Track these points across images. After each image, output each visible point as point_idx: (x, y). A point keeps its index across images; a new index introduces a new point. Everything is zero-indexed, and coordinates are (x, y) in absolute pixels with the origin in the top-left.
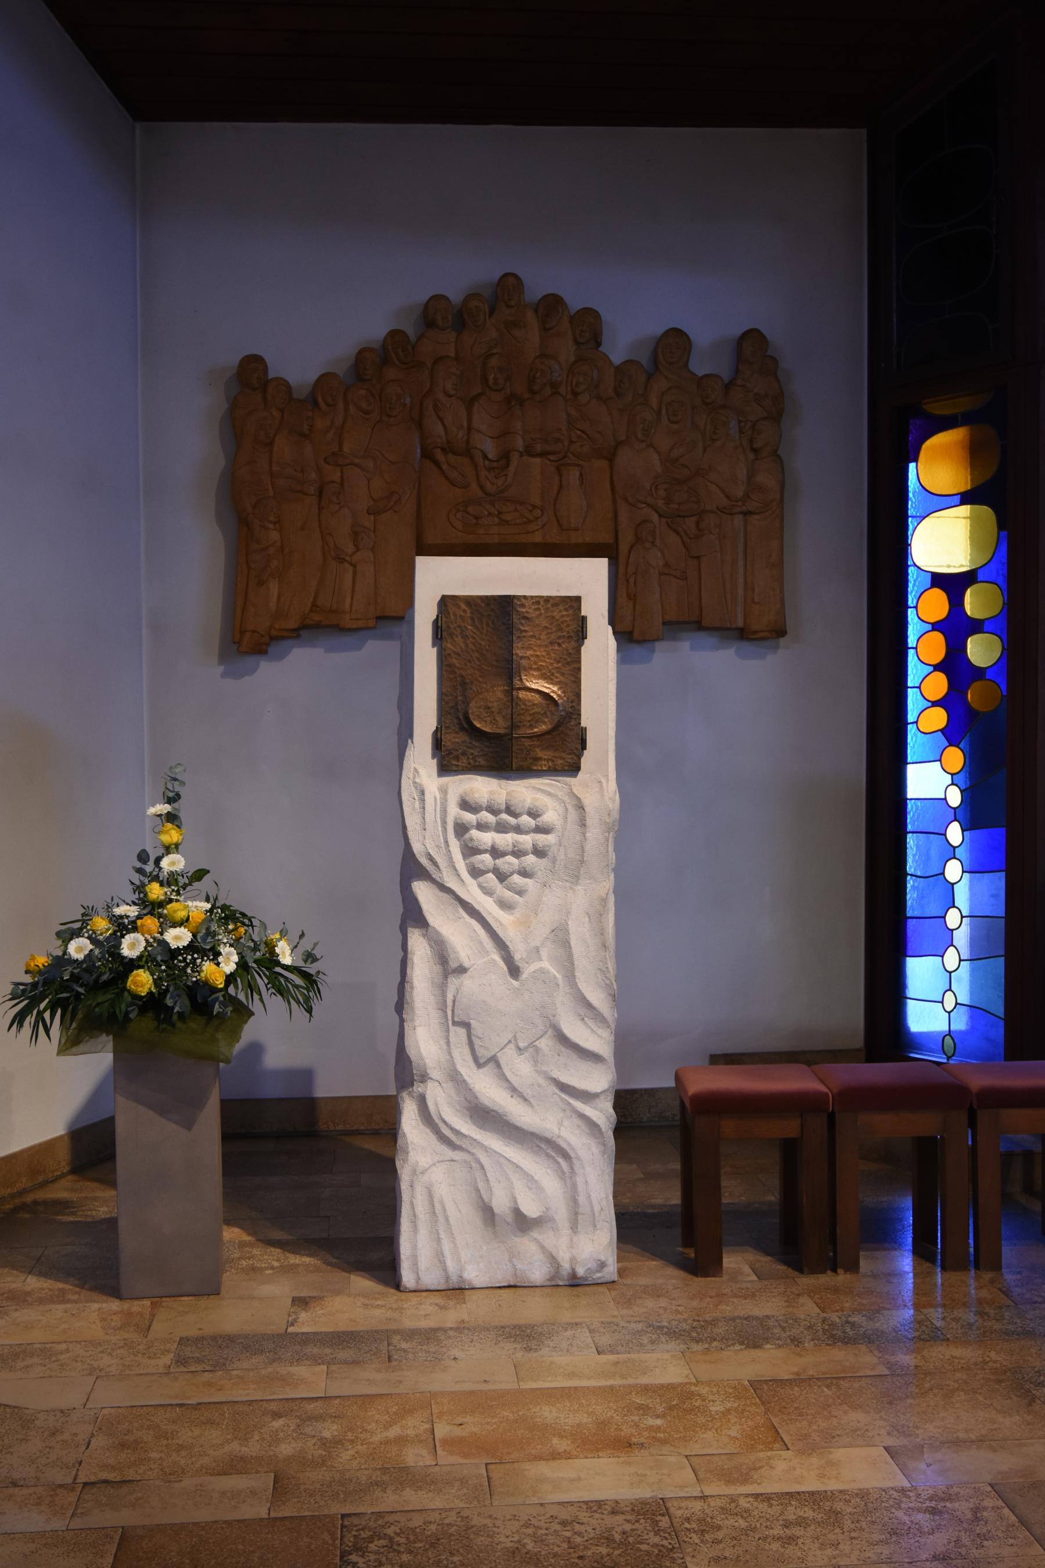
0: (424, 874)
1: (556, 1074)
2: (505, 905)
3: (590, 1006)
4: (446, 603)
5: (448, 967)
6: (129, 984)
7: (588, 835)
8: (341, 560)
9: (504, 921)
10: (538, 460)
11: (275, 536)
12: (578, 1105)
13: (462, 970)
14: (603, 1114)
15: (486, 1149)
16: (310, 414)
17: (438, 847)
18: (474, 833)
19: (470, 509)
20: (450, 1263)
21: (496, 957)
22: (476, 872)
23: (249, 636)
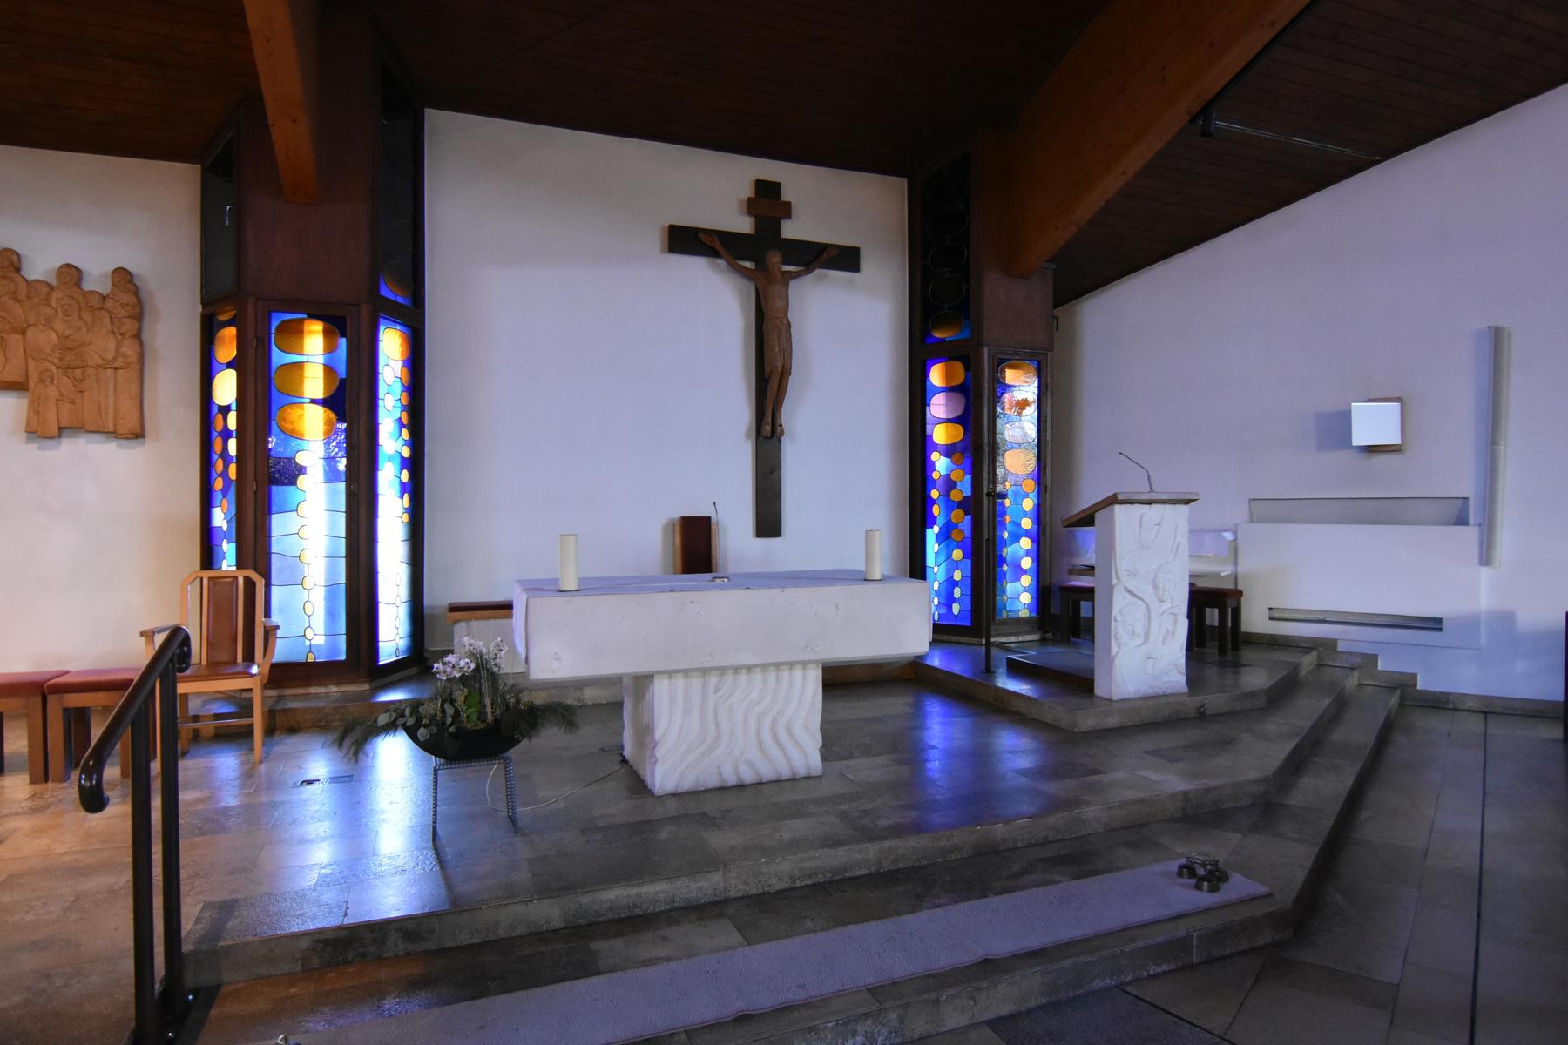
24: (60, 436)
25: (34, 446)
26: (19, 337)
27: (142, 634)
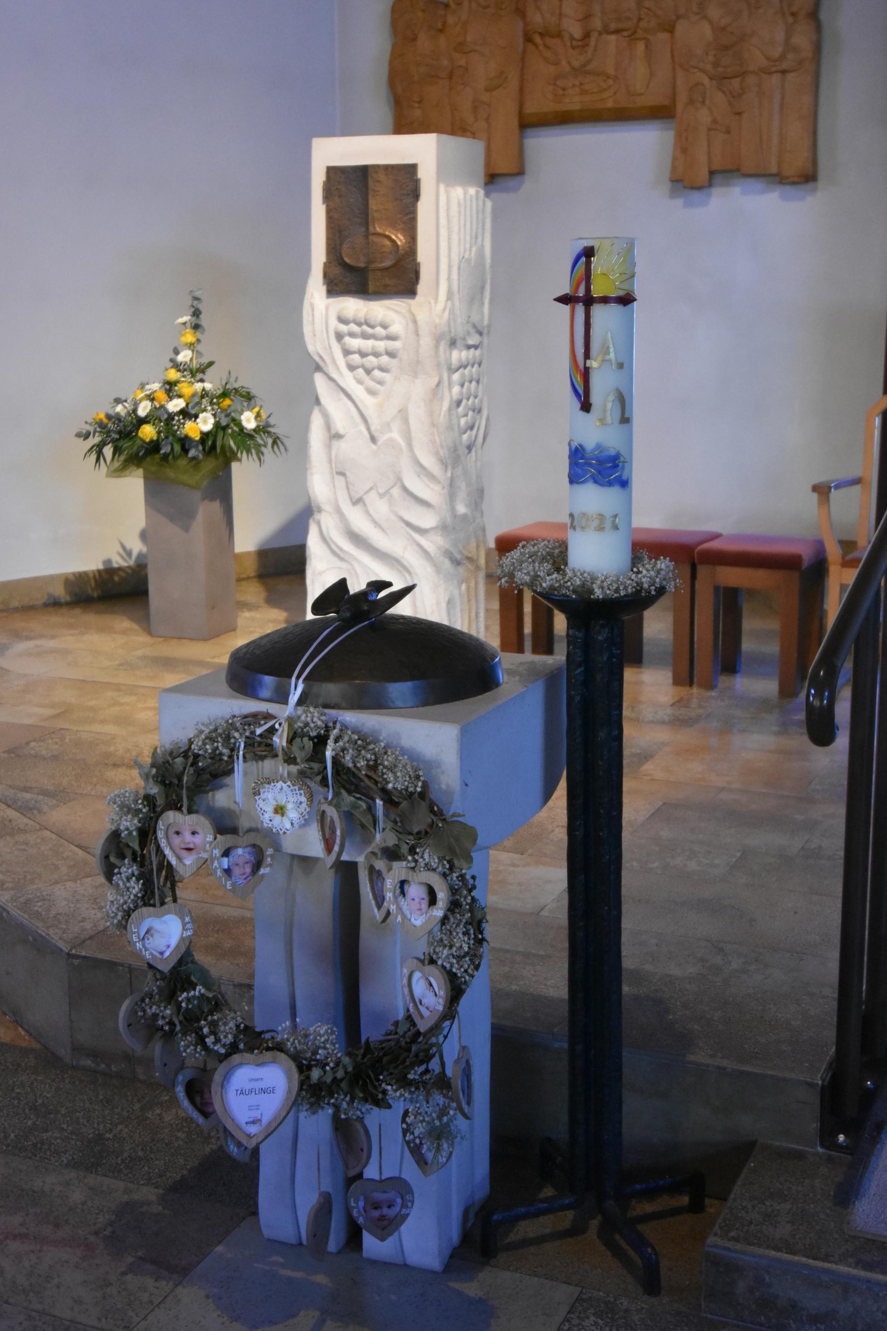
0: (318, 368)
2: (372, 392)
3: (422, 466)
4: (333, 172)
6: (140, 434)
7: (421, 342)
9: (368, 403)
10: (613, 38)
12: (417, 537)
15: (359, 562)
16: (443, 12)
17: (325, 348)
18: (347, 339)
19: (558, 83)
21: (363, 428)
22: (352, 368)
24: (710, 185)
25: (679, 202)
26: (665, 36)
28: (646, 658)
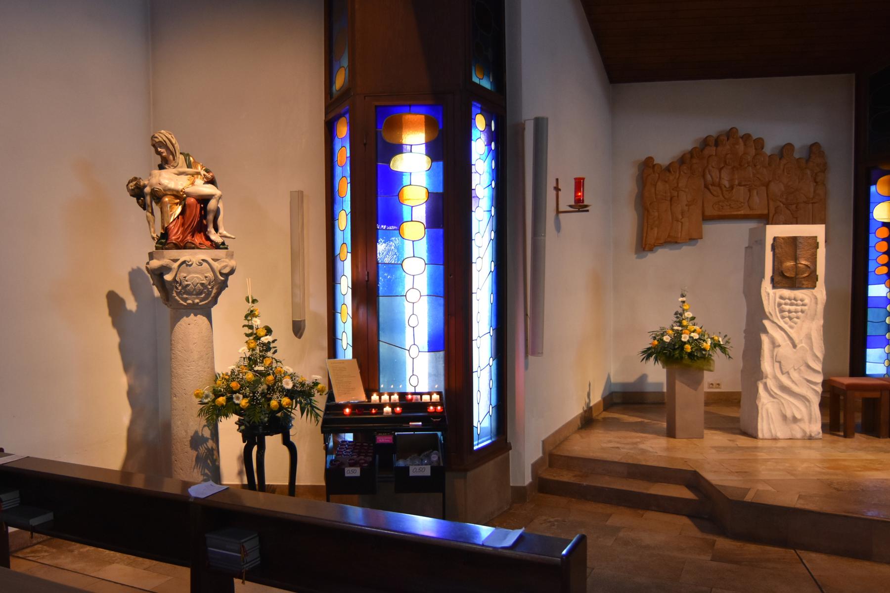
0: (767, 318)
1: (806, 377)
2: (791, 327)
3: (817, 357)
5: (774, 344)
8: (678, 221)
11: (656, 214)
13: (779, 346)
14: (819, 389)
20: (773, 431)
22: (783, 317)
23: (645, 245)
27: (648, 353)
28: (678, 433)
